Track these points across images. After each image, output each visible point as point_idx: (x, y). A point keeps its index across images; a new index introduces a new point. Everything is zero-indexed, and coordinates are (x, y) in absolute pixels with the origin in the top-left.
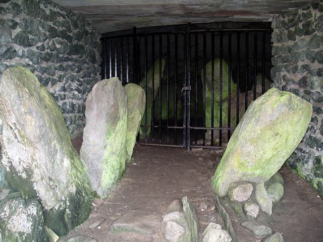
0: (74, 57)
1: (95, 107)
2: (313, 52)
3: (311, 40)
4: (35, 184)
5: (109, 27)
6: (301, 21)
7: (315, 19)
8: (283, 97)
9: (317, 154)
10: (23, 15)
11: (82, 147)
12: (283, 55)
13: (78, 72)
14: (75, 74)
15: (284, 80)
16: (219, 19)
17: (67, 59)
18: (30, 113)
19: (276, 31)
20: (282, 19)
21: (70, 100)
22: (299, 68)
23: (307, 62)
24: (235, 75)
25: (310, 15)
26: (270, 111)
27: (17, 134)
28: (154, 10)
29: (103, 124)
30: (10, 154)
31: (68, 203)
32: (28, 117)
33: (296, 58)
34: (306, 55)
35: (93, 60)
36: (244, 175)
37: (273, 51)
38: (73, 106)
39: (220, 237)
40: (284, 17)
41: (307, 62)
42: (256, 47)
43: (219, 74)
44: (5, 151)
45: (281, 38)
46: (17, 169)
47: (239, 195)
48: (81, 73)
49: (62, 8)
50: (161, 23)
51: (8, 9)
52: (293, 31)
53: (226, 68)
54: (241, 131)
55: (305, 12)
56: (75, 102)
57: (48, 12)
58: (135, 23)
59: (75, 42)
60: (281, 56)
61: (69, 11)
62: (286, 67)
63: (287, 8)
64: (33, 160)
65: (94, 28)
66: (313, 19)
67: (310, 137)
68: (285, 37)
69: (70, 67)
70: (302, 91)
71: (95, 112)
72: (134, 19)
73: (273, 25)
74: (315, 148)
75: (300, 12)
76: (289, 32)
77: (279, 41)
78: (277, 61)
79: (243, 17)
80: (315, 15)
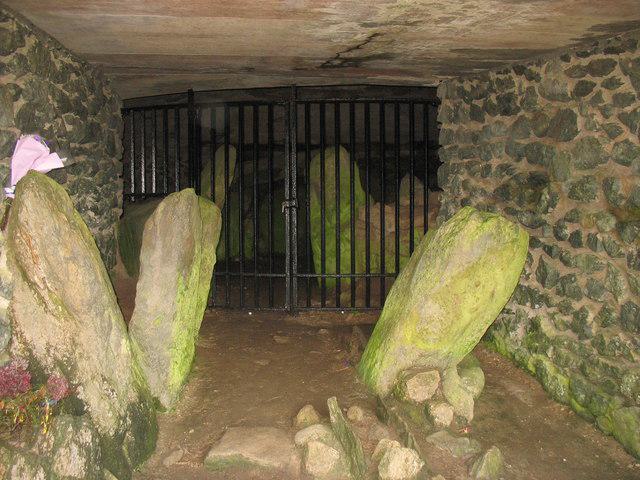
1: (159, 244)
2: (518, 144)
3: (516, 124)
4: (80, 389)
5: (144, 88)
7: (520, 91)
8: (489, 223)
9: (532, 315)
10: (29, 76)
11: (133, 318)
12: (461, 146)
13: (93, 174)
16: (348, 80)
17: (81, 151)
18: (74, 259)
19: (446, 103)
20: (458, 84)
22: (494, 169)
25: (510, 83)
26: (466, 247)
27: (47, 298)
29: (171, 270)
30: (28, 336)
31: (129, 421)
32: (72, 267)
33: (488, 152)
34: (507, 147)
36: (421, 355)
39: (407, 460)
40: (462, 82)
41: (507, 160)
42: (397, 128)
43: (337, 170)
44: (18, 329)
45: (457, 116)
46: (44, 363)
47: (417, 391)
48: (96, 176)
50: (243, 85)
51: (10, 65)
52: (481, 106)
55: (501, 77)
57: (58, 66)
60: (456, 147)
61: (84, 62)
62: (468, 167)
63: (470, 68)
64: (74, 343)
65: (113, 92)
66: (515, 90)
69: (83, 165)
71: (158, 254)
73: (441, 93)
74: (528, 304)
75: (493, 76)
76: (473, 107)
77: (452, 121)
78: (449, 156)
79: (392, 78)
80: (520, 86)
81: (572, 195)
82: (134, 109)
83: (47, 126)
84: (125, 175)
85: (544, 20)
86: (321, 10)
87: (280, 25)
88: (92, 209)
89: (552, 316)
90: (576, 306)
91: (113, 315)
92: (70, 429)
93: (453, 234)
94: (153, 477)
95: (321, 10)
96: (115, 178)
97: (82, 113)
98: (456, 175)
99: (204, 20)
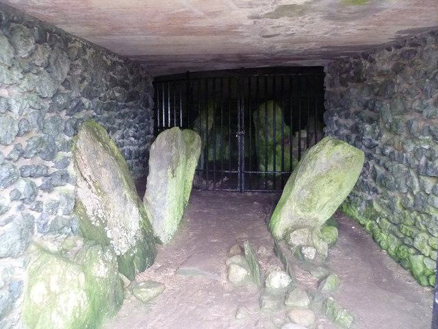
0: (130, 103)
5: (163, 71)
6: (353, 69)
9: (369, 198)
13: (134, 118)
14: (132, 120)
15: (337, 124)
17: (125, 107)
18: (105, 166)
19: (328, 75)
21: (128, 147)
23: (358, 108)
24: (287, 120)
28: (209, 58)
32: (104, 170)
35: (147, 105)
37: (326, 96)
38: (130, 152)
43: (273, 118)
45: (334, 83)
48: (136, 118)
49: (120, 57)
53: (279, 111)
54: (297, 178)
55: (356, 60)
56: (131, 148)
58: (190, 68)
59: (131, 89)
61: (126, 60)
62: (338, 113)
65: (147, 73)
67: (362, 181)
68: (337, 81)
70: (354, 136)
72: (188, 65)
73: (326, 69)
81: (390, 130)
82: (158, 81)
83: (102, 95)
84: (155, 118)
85: (366, 29)
86: (236, 30)
87: (218, 38)
88: (133, 137)
89: (378, 201)
90: (391, 194)
91: (128, 193)
92: (99, 253)
93: (316, 152)
94: (435, 304)
95: (236, 30)
96: (149, 119)
97: (126, 86)
98: (335, 119)
99: (177, 38)
